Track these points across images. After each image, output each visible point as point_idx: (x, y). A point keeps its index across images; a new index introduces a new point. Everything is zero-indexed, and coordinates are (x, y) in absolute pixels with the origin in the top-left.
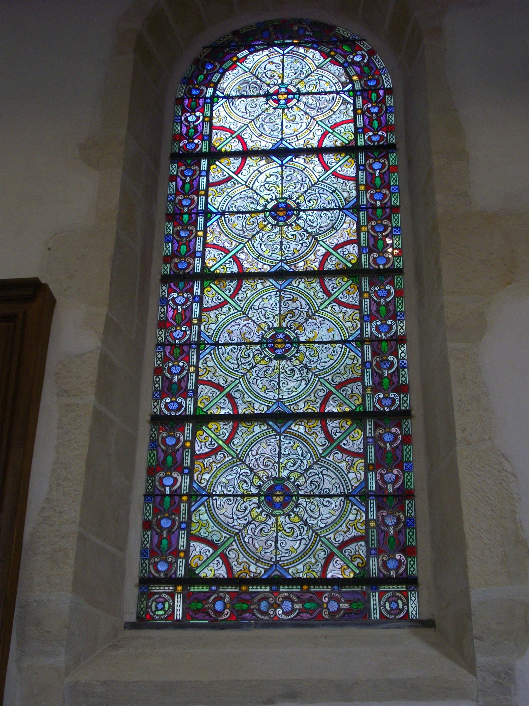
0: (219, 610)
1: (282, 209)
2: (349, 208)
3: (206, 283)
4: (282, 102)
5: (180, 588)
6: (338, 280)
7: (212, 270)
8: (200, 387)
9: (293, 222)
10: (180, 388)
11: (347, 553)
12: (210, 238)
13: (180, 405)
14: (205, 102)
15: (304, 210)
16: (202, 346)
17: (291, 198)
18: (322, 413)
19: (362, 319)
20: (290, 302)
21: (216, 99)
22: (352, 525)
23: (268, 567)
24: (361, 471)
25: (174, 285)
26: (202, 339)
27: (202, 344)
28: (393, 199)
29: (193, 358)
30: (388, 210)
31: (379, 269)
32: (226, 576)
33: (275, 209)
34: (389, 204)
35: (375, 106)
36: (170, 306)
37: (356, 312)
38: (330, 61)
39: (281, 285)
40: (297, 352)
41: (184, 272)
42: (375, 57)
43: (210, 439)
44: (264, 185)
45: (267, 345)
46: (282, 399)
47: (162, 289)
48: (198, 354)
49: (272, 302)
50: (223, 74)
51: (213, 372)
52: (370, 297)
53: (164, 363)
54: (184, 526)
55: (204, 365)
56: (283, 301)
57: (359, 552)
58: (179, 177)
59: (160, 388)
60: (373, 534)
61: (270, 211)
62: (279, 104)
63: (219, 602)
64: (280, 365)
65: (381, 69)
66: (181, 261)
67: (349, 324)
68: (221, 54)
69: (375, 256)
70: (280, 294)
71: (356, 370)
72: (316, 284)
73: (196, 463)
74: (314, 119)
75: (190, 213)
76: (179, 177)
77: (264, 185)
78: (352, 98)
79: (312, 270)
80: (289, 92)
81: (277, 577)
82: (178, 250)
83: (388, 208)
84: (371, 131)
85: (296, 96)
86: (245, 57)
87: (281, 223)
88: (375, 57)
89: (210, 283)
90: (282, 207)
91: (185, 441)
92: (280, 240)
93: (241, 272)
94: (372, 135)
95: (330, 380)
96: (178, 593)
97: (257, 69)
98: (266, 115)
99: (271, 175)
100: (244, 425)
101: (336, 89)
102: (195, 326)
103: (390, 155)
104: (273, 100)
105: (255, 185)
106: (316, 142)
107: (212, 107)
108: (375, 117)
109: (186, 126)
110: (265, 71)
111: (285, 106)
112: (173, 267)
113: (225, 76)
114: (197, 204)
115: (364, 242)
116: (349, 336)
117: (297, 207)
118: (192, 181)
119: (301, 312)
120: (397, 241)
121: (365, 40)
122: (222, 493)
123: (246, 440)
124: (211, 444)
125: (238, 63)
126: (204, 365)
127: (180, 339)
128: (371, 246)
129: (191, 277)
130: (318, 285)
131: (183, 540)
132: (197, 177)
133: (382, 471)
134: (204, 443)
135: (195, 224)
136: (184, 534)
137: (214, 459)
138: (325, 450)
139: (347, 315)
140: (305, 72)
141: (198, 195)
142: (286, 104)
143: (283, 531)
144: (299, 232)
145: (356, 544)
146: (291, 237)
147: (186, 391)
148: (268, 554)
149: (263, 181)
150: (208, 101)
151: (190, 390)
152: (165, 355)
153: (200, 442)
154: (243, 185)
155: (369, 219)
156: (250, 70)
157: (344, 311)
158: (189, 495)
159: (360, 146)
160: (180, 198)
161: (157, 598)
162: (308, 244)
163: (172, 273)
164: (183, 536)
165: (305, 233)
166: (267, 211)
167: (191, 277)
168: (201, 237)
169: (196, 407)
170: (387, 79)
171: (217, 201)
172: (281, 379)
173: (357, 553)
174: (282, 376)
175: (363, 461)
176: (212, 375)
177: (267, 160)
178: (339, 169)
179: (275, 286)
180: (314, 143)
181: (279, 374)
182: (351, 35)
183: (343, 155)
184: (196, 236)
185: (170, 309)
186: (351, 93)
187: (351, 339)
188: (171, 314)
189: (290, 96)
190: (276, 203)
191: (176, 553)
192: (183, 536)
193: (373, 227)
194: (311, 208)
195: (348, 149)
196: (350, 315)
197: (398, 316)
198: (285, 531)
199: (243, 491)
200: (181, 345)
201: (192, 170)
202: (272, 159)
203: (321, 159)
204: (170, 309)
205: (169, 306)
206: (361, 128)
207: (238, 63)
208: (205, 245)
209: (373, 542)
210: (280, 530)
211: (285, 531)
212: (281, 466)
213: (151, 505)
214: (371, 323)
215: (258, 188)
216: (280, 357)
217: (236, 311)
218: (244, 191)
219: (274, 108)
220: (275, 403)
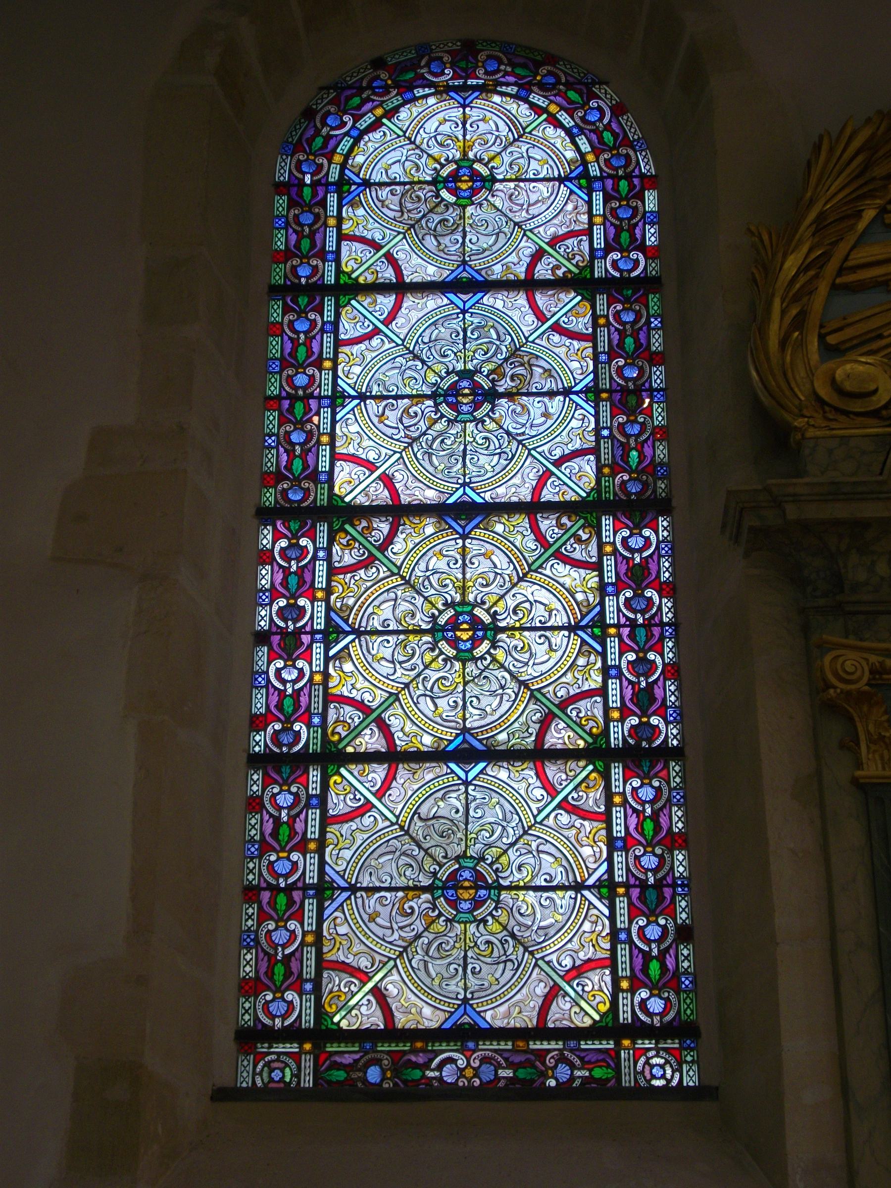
0: (373, 1081)
1: (467, 884)
2: (581, 391)
3: (343, 300)
4: (465, 906)
5: (308, 1046)
6: (569, 763)
7: (347, 499)
8: (338, 464)
9: (484, 416)
10: (293, 833)
11: (562, 249)
12: (347, 227)
13: (295, 864)
14: (313, 641)
15: (509, 888)
16: (328, 893)
17: (482, 859)
18: (535, 503)
19: (611, 842)
20: (481, 124)
21: (339, 401)
22: (587, 940)
23: (453, 1010)
24: (600, 844)
25: (283, 524)
26: (327, 878)
27: (328, 889)
28: (654, 377)
29: (329, 314)
30: (636, 181)
31: (652, 1026)
32: (382, 1027)
33: (455, 177)
34: (647, 385)
35: (635, 479)
36: (268, 812)
37: (600, 826)
38: (545, 120)
39: (465, 303)
40: (496, 908)
41: (299, 505)
42: (625, 117)
43: (353, 790)
44: (435, 137)
45: (443, 892)
46: (471, 483)
47: (252, 779)
48: (321, 910)
49: (451, 331)
50: (357, 140)
51: (359, 440)
52: (615, 552)
53: (259, 924)
54: (328, 327)
55: (331, 931)
56: (469, 122)
57: (592, 712)
58: (287, 334)
59: (257, 838)
60: (617, 783)
61: (446, 180)
62: (459, 413)
63: (372, 1068)
64: (465, 362)
65: (634, 140)
66: (302, 263)
67: (575, 365)
68: (356, 101)
69: (615, 257)
70: (464, 543)
71: (587, 437)
72: (521, 299)
73: (328, 829)
74: (524, 445)
75: (314, 185)
76: (291, 227)
77: (435, 137)
78: (606, 902)
79: (523, 748)
80: (476, 623)
81: (467, 1026)
82: (298, 246)
83: (636, 177)
84: (622, 357)
85: (489, 633)
86: (396, 110)
87: (463, 202)
88: (625, 117)
89: (344, 523)
90: (464, 622)
91: (312, 673)
92: (463, 954)
93: (390, 1027)
94: (624, 366)
95: (546, 452)
96: (306, 1054)
97: (418, 132)
98: (431, 936)
99: (446, 120)
100: (406, 766)
101: (559, 174)
102: (317, 687)
103: (651, 296)
104: (446, 899)
105: (419, 136)
106: (523, 269)
107: (334, 414)
108: (625, 224)
109: (295, 231)
110: (428, 574)
111: (468, 201)
112: (284, 384)
113: (362, 143)
114: (304, 873)
115: (606, 455)
116: (576, 384)
117: (492, 174)
118: (293, 819)
119: (497, 137)
120: (653, 235)
121: (607, 83)
122: (371, 885)
123: (410, 793)
124: (355, 798)
125: (385, 121)
126: (331, 931)
127: (286, 876)
128: (611, 192)
129: (317, 290)
130: (532, 773)
131: (308, 1011)
132: (314, 446)
133: (637, 851)
134: (342, 797)
135: (323, 204)
136: (313, 904)
137: (360, 825)
138: (543, 809)
139: (572, 351)
140: (504, 349)
141: (324, 260)
142: (471, 911)
143: (475, 949)
144: (496, 433)
145: (589, 700)
146: (480, 442)
147: (305, 841)
148: (453, 474)
149: (433, 131)
150: (326, 402)
151: (329, 252)
152: (260, 909)
153: (337, 794)
154: (398, 345)
155: (607, 199)
156: (405, 132)
157: (577, 824)
158: (325, 633)
159: (623, 1024)
160: (290, 372)
161: (273, 1061)
162: (513, 696)
163: (260, 1027)
164: (325, 454)
165: (505, 436)
166: (440, 182)
167: (317, 290)
168: (319, 684)
169: (339, 271)
170: (646, 160)
171: (353, 371)
172: (469, 960)
173: (589, 713)
174: (470, 954)
175: (591, 345)
176: (356, 446)
177: (438, 525)
178: (564, 318)
179: (455, 530)
180: (525, 495)
181: (466, 952)
182: (585, 75)
183: (573, 294)
184: (325, 225)
185: (266, 817)
186: (604, 891)
187: (577, 388)
188: (269, 827)
189: (482, 892)
190: (455, 166)
191: (322, 255)
192: (325, 454)
193: (621, 426)
194: (522, 884)
195: (581, 283)
196: (590, 833)
197: (663, 549)
198: (477, 443)
199: (406, 881)
200: (289, 889)
201: (308, 319)
202: (447, 523)
203: (540, 769)
204: (266, 817)
205: (265, 812)
206: (612, 584)
207: (385, 121)
208: (335, 457)
209: (623, 952)
210: (470, 947)
211: (479, 948)
212: (469, 837)
213: (285, 198)
214: (617, 595)
215: (425, 141)
216: (465, 374)
217: (394, 345)
218: (400, 356)
219: (447, 920)
220: (459, 1006)
